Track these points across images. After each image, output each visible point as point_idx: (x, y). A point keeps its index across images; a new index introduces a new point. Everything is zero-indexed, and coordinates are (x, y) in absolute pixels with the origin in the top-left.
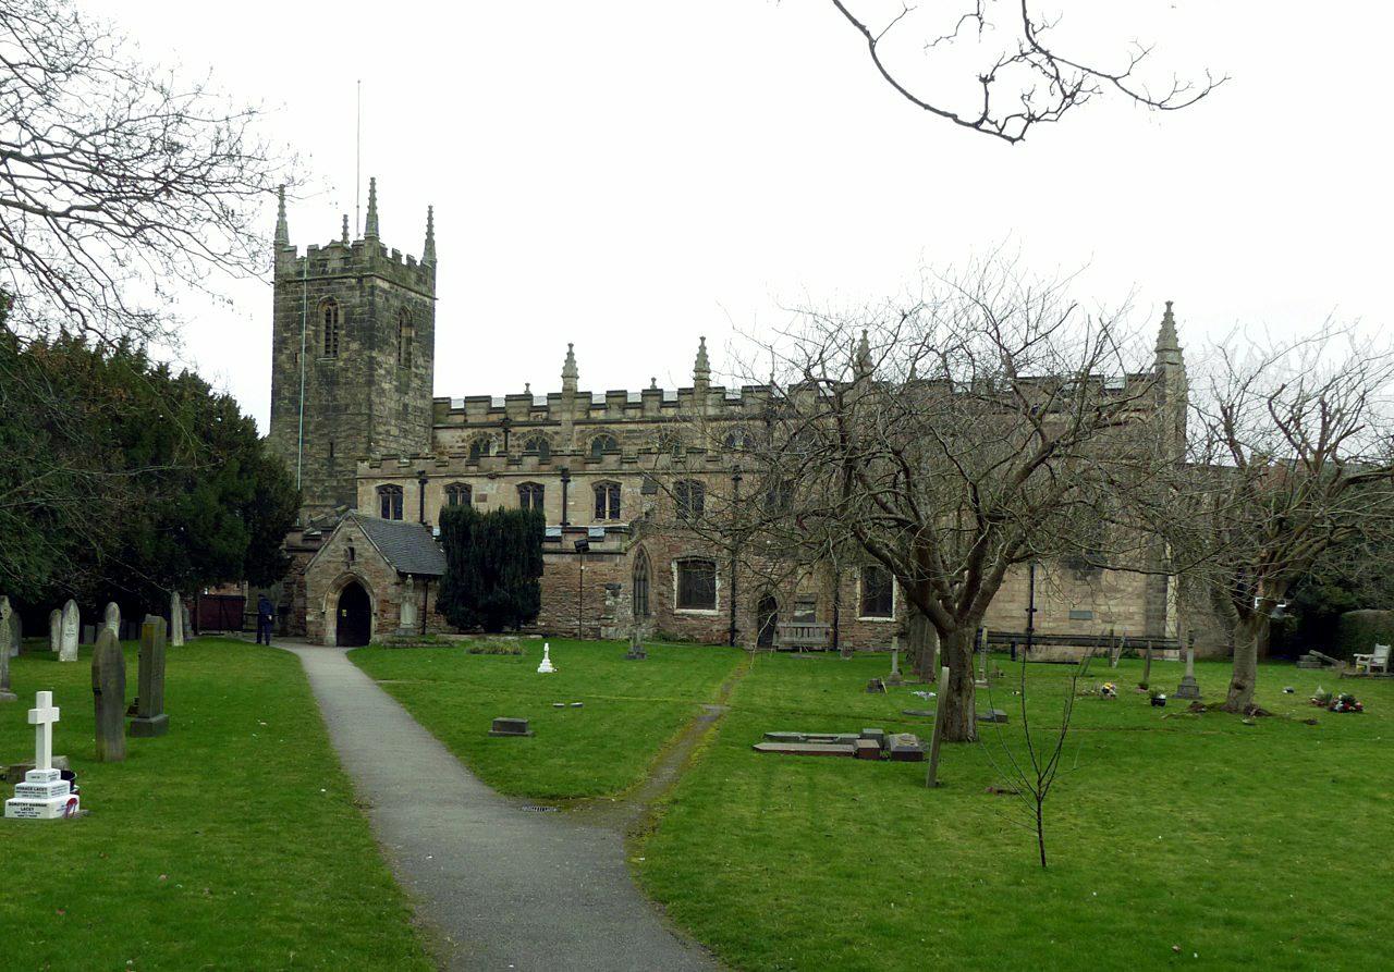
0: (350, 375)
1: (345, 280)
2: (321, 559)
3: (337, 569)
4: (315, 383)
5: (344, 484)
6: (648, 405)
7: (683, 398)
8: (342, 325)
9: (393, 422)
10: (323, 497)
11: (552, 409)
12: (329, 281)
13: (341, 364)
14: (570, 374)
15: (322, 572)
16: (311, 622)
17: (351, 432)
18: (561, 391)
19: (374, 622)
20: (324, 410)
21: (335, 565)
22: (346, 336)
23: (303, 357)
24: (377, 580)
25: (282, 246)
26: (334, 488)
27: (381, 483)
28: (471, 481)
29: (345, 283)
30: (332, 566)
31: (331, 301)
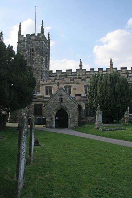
0: (37, 62)
6: (100, 72)
7: (108, 70)
11: (77, 72)
13: (34, 59)
14: (81, 65)
18: (79, 69)
19: (69, 121)
22: (36, 53)
24: (71, 108)
25: (20, 34)
27: (46, 86)
28: (72, 85)
30: (55, 103)
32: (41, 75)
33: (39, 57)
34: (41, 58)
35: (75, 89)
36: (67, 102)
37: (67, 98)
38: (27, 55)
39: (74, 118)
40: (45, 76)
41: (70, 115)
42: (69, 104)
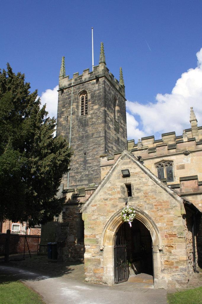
0: (94, 120)
1: (90, 82)
2: (98, 198)
3: (114, 206)
4: (76, 128)
5: (92, 172)
8: (90, 100)
9: (114, 144)
10: (81, 180)
12: (83, 83)
15: (99, 210)
16: (89, 260)
17: (95, 146)
20: (81, 138)
21: (111, 202)
22: (92, 103)
23: (71, 118)
24: (160, 213)
26: (87, 175)
29: (90, 83)
30: (109, 203)
31: (84, 92)
32: (103, 146)
33: (98, 109)
34: (102, 111)
35: (182, 167)
36: (146, 195)
37: (145, 184)
38: (76, 110)
39: (173, 251)
40: (115, 148)
41: (159, 240)
42: (152, 201)
